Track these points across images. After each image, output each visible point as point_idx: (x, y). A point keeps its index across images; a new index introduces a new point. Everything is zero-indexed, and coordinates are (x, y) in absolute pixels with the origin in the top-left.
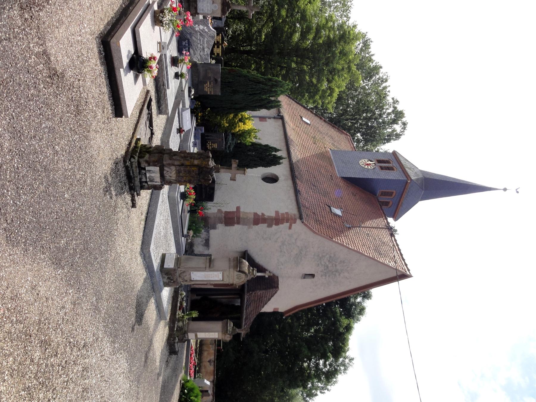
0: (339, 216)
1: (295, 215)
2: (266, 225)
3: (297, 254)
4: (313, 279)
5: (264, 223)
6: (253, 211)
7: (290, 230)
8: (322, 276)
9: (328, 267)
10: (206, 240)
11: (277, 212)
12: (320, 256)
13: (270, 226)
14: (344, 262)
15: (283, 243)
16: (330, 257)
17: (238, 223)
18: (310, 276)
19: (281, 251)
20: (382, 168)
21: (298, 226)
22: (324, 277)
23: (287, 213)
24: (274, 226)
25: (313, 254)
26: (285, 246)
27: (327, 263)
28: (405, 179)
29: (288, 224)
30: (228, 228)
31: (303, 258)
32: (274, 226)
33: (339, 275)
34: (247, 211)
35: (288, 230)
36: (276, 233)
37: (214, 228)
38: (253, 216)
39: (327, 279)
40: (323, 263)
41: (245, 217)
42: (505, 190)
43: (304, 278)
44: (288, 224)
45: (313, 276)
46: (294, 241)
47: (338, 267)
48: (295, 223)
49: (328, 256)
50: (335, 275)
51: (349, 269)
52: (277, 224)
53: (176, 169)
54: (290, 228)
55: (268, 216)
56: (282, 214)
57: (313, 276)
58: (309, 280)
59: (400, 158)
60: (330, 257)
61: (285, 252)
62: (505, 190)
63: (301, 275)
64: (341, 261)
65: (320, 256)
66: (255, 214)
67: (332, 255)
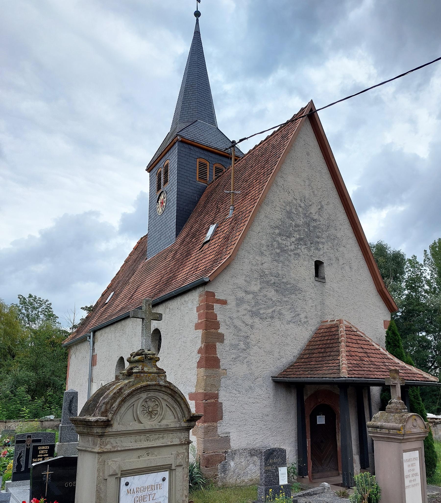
0: (217, 227)
1: (200, 296)
2: (218, 344)
3: (277, 291)
4: (325, 264)
5: (215, 348)
6: (195, 371)
7: (228, 301)
8: (319, 250)
9: (300, 239)
10: (252, 455)
11: (197, 327)
12: (278, 251)
13: (221, 338)
14: (289, 213)
15: (254, 314)
16: (280, 234)
17: (216, 396)
18: (320, 268)
19: (272, 317)
20: (166, 182)
21: (221, 290)
22: (321, 246)
23: (198, 309)
24: (220, 331)
25: (276, 263)
26: (261, 312)
27: (293, 239)
28: (177, 144)
29: (217, 307)
30: (226, 416)
31: (284, 280)
32: (220, 331)
33: (315, 220)
34: (194, 379)
35: (228, 307)
36: (236, 327)
37: (227, 440)
38: (202, 370)
39: (323, 240)
40: (292, 247)
41: (203, 384)
42: (197, 14)
43: (324, 278)
44: (217, 307)
45: (318, 265)
46: (251, 296)
47: (301, 221)
48: (213, 294)
49: (279, 239)
50: (315, 227)
51: (302, 205)
52: (217, 325)
53: (435, 469)
54: (224, 302)
55: (202, 342)
56: (200, 317)
57: (318, 265)
58: (327, 271)
59: (154, 159)
60: (280, 234)
61: (274, 311)
62: (197, 14)
63: (318, 284)
64: (289, 218)
65: (278, 251)
66: (199, 365)
67: (277, 231)
